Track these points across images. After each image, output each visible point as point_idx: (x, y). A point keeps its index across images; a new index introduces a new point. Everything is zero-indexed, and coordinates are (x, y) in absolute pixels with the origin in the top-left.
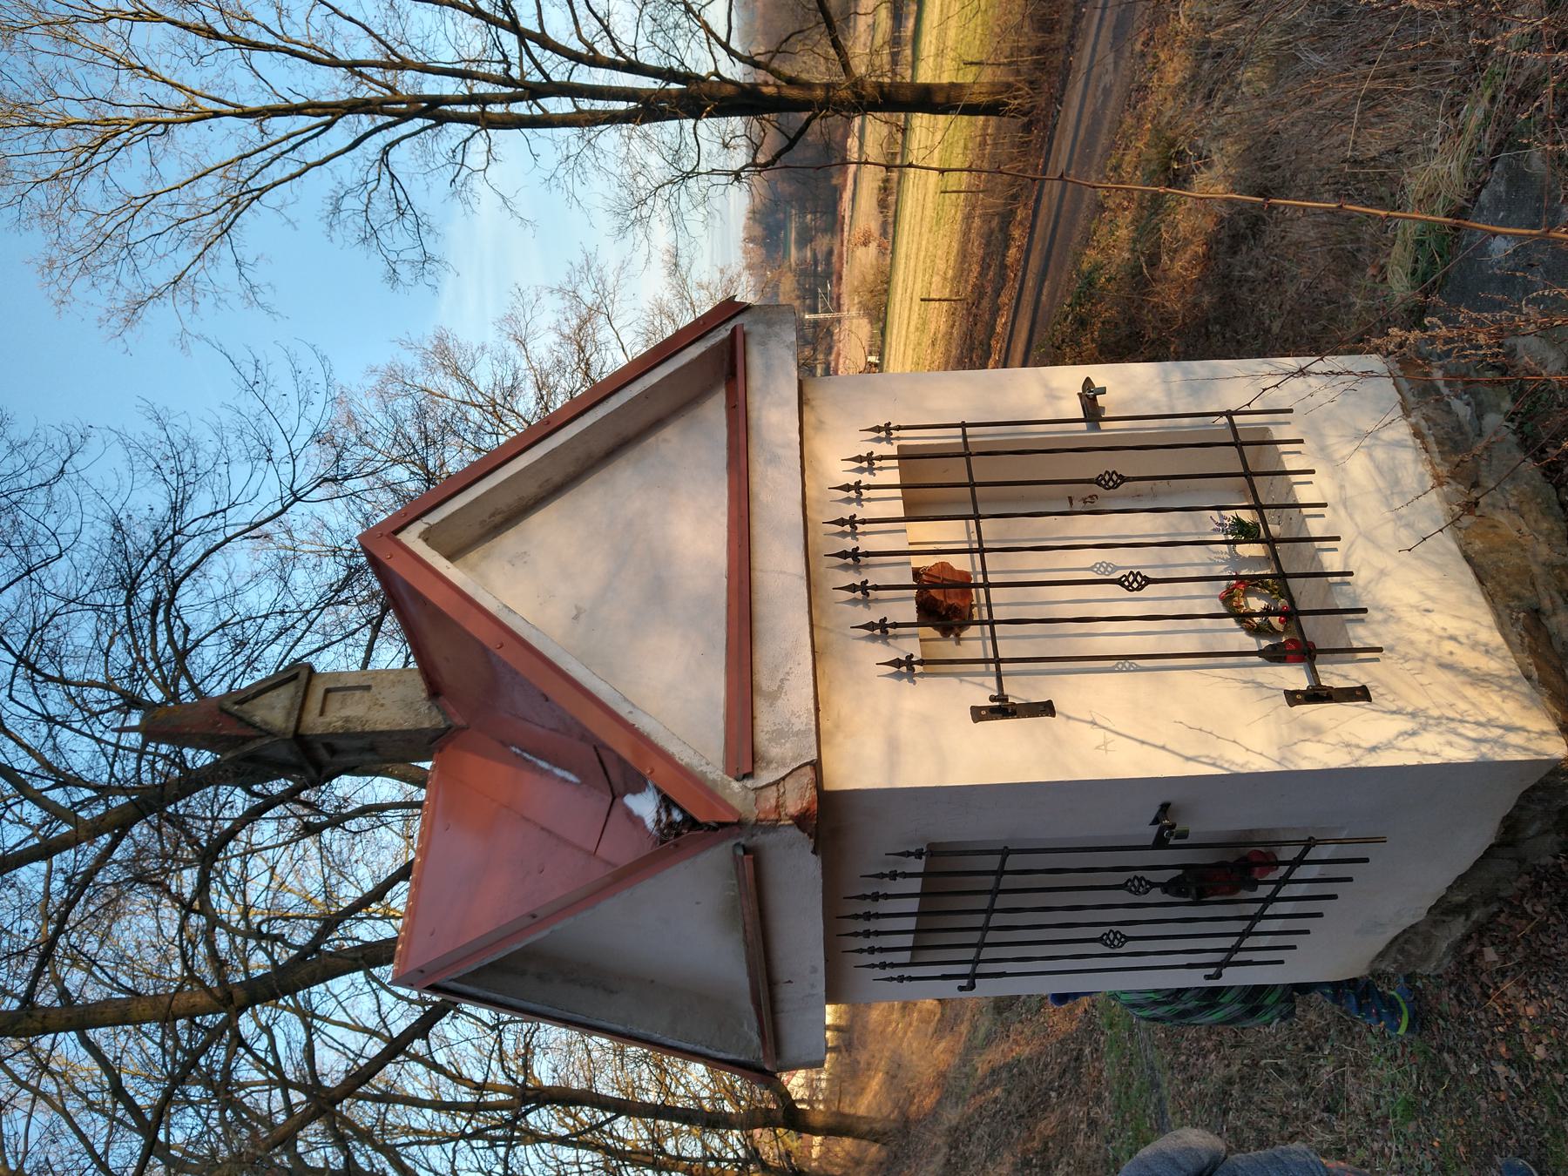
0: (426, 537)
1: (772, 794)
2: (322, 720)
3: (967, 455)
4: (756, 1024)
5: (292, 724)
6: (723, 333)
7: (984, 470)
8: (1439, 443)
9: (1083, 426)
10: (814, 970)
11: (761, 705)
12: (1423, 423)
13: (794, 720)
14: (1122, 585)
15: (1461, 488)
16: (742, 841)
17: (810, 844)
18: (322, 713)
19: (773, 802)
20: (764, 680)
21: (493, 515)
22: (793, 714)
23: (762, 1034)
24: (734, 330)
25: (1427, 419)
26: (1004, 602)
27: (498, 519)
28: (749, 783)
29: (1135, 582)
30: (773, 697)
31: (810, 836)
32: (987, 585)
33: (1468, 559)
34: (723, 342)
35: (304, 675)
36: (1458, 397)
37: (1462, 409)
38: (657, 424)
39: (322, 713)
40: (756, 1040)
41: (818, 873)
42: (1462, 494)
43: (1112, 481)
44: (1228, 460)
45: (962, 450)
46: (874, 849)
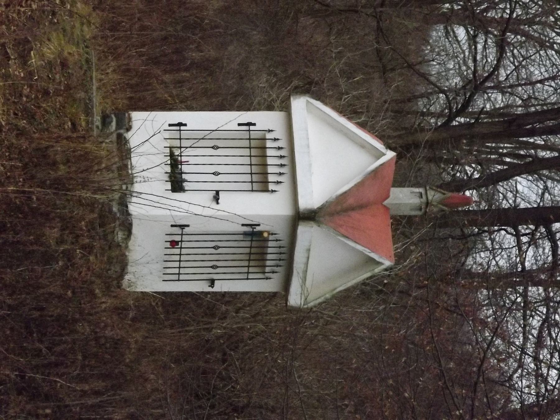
29: (216, 174)
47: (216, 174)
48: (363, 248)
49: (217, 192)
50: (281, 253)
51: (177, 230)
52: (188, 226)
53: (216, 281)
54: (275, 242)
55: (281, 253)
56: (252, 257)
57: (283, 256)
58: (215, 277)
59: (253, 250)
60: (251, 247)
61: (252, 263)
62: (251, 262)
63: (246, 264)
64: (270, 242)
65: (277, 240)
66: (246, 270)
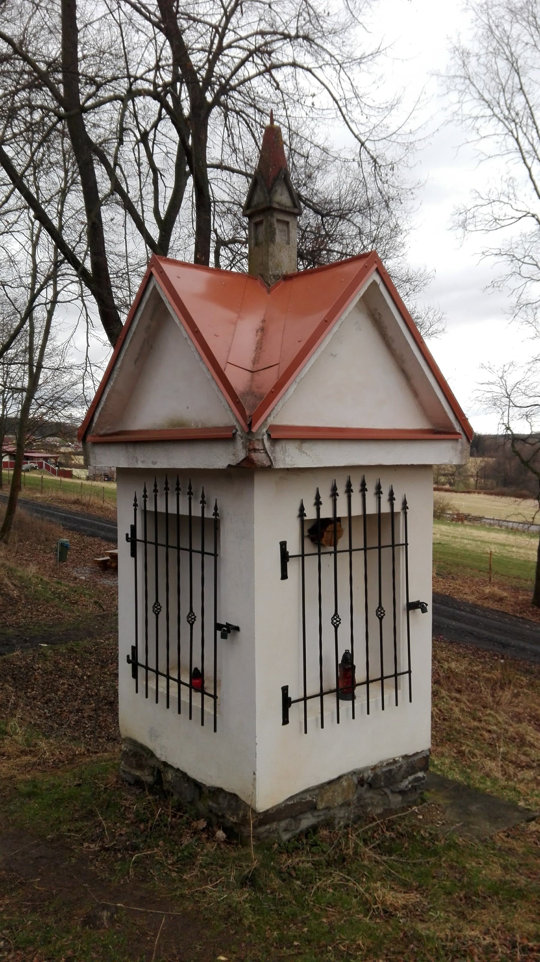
0: (374, 283)
1: (260, 447)
2: (275, 220)
3: (393, 546)
4: (109, 432)
5: (276, 206)
6: (458, 429)
7: (386, 553)
8: (390, 771)
9: (405, 602)
10: (154, 463)
11: (297, 444)
12: (399, 764)
13: (290, 458)
14: (335, 615)
15: (370, 779)
16: (239, 433)
17: (233, 463)
18: (279, 221)
19: (257, 447)
20: (306, 446)
21: (379, 314)
22: (293, 457)
23: (105, 435)
24: (459, 434)
25: (400, 767)
26: (327, 561)
27: (377, 316)
28: (265, 437)
29: (336, 622)
30: (300, 449)
31: (239, 464)
32: (335, 553)
33: (340, 778)
34: (454, 429)
35: (296, 211)
36: (409, 783)
37: (405, 784)
38: (415, 394)
39: (279, 221)
40: (102, 432)
41: (216, 467)
42: (368, 779)
43: (380, 613)
44: (389, 671)
45: (396, 543)
46: (461, 486)
47: (336, 622)
48: (362, 294)
49: (218, 627)
50: (167, 489)
51: (295, 711)
52: (285, 690)
53: (218, 622)
54: (169, 495)
55: (167, 489)
56: (173, 542)
57: (172, 485)
58: (402, 603)
59: (197, 546)
60: (191, 551)
61: (184, 544)
62: (194, 548)
63: (185, 556)
64: (170, 511)
65: (145, 496)
66: (197, 558)
